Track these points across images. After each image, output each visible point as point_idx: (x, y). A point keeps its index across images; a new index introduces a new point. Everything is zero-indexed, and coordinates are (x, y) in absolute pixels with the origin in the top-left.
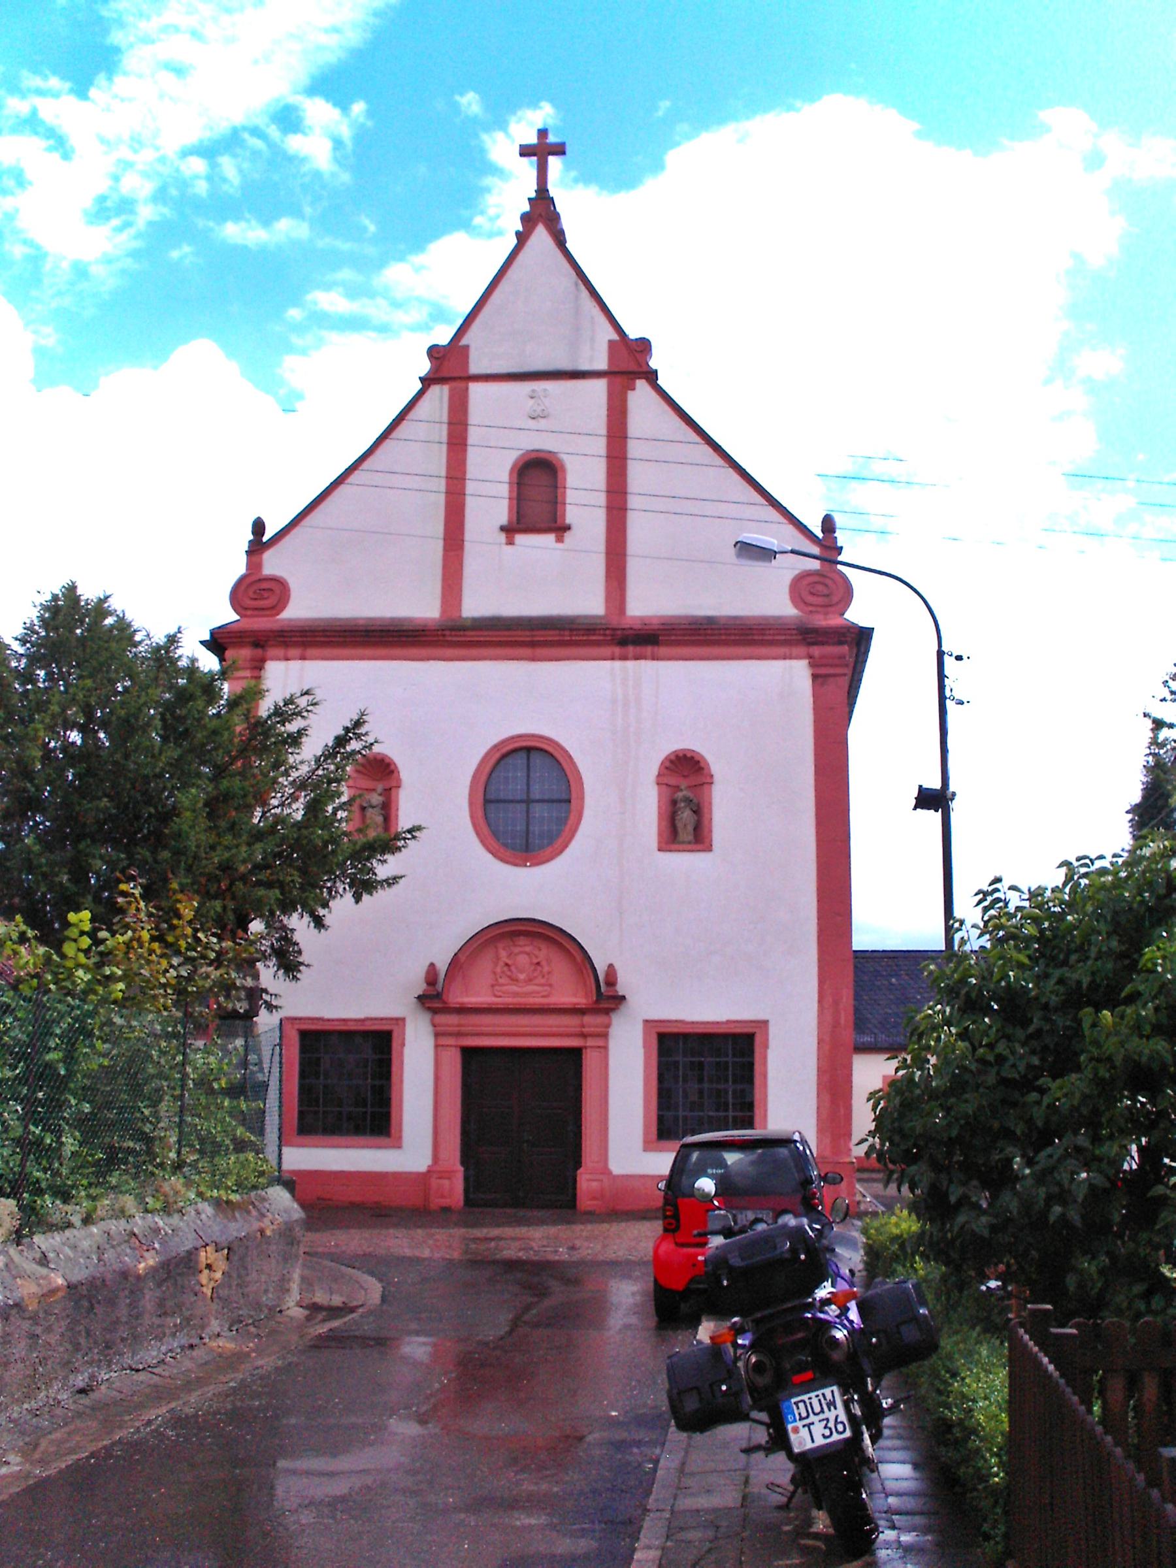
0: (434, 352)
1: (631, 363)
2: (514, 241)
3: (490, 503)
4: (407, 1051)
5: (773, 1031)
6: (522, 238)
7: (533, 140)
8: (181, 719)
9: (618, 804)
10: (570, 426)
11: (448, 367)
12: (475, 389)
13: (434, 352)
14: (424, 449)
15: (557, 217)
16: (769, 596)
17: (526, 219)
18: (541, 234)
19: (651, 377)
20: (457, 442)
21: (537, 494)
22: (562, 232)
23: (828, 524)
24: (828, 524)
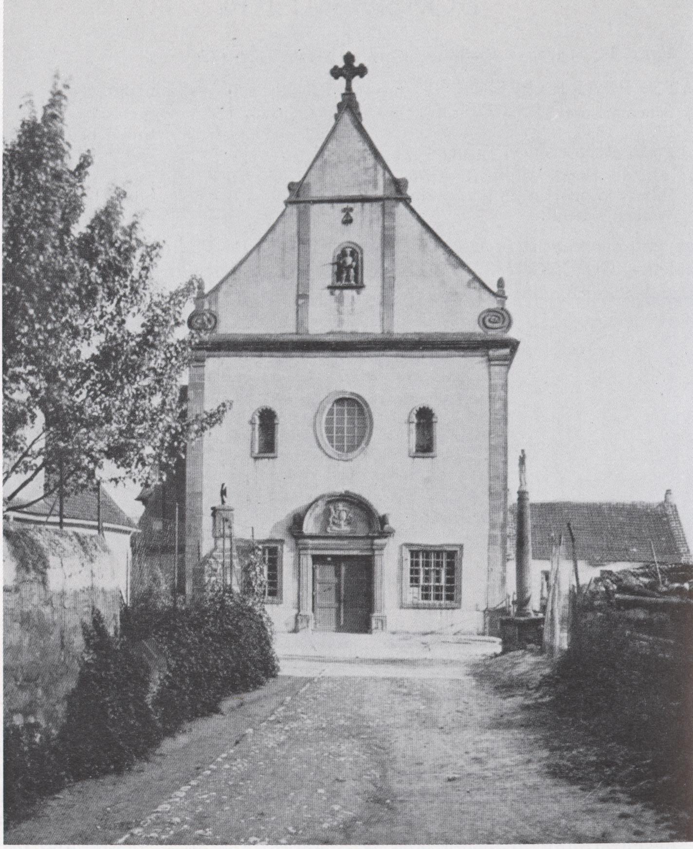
0: (291, 187)
1: (398, 191)
2: (332, 122)
3: (322, 274)
4: (361, 329)
5: (465, 551)
6: (337, 117)
7: (341, 64)
8: (156, 335)
9: (392, 431)
10: (365, 231)
11: (298, 196)
12: (315, 209)
13: (291, 187)
14: (291, 225)
15: (356, 105)
16: (466, 323)
17: (340, 106)
18: (347, 118)
19: (406, 201)
20: (303, 240)
21: (347, 272)
22: (359, 114)
23: (501, 283)
24: (501, 283)
